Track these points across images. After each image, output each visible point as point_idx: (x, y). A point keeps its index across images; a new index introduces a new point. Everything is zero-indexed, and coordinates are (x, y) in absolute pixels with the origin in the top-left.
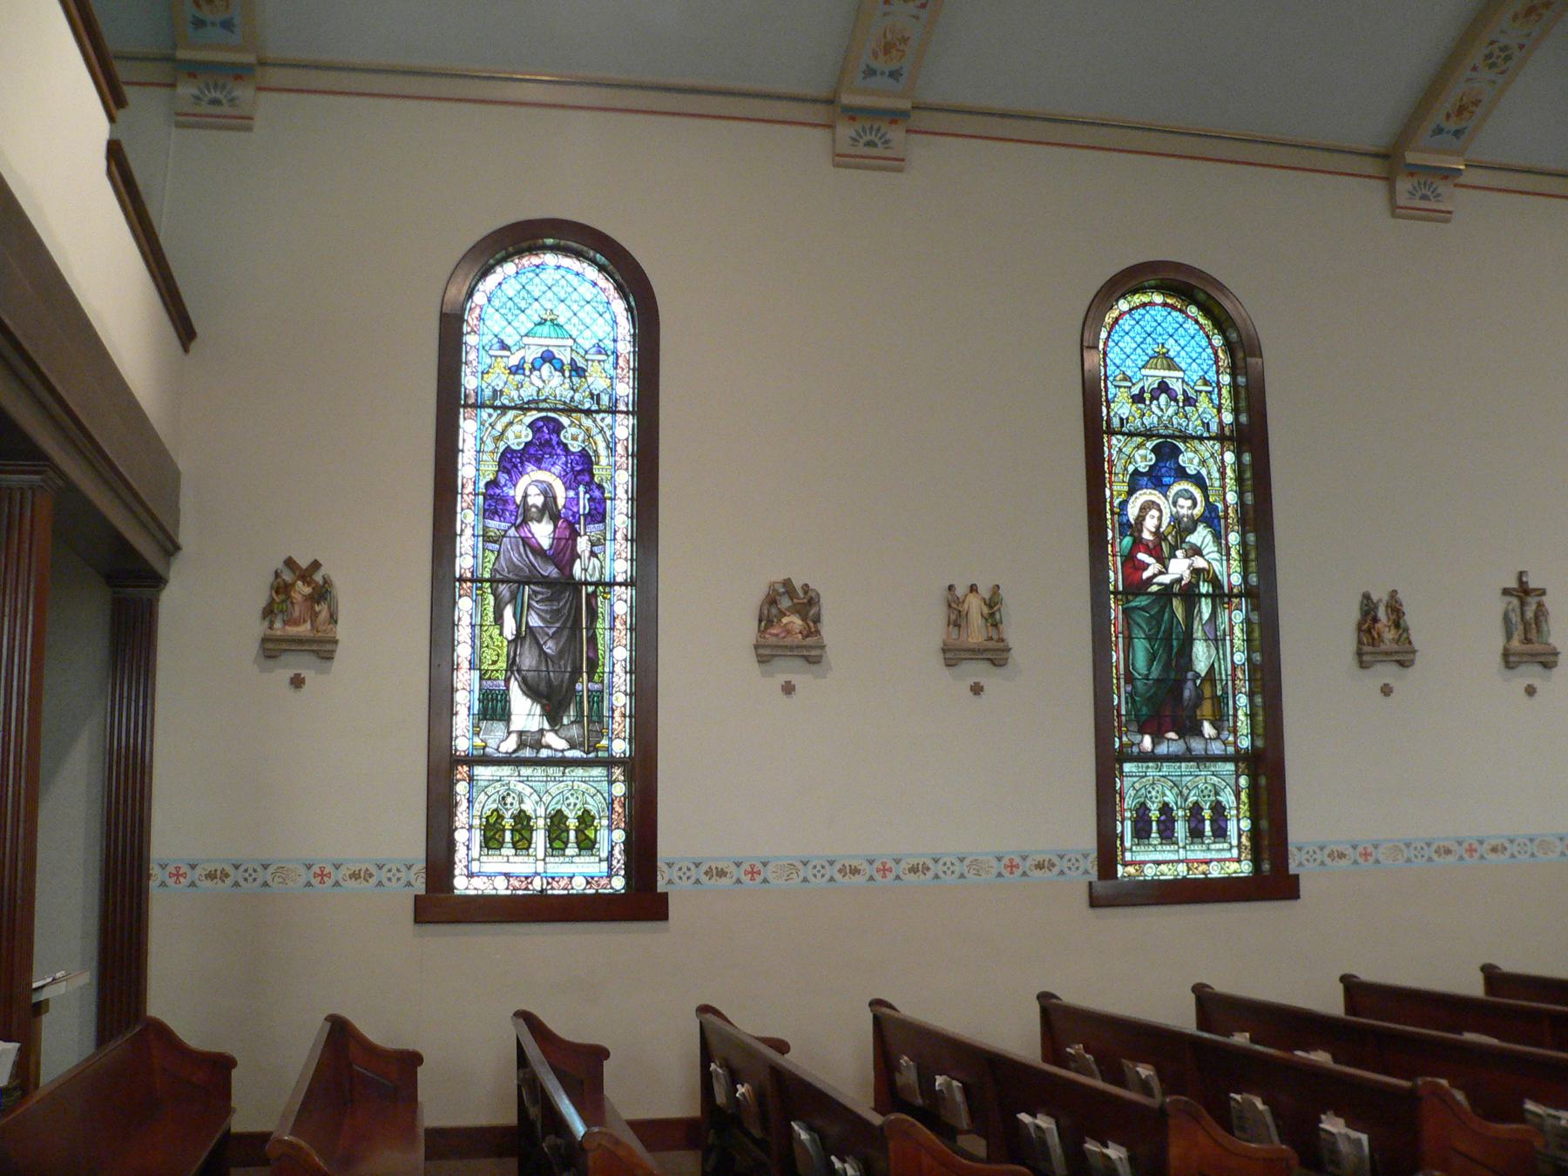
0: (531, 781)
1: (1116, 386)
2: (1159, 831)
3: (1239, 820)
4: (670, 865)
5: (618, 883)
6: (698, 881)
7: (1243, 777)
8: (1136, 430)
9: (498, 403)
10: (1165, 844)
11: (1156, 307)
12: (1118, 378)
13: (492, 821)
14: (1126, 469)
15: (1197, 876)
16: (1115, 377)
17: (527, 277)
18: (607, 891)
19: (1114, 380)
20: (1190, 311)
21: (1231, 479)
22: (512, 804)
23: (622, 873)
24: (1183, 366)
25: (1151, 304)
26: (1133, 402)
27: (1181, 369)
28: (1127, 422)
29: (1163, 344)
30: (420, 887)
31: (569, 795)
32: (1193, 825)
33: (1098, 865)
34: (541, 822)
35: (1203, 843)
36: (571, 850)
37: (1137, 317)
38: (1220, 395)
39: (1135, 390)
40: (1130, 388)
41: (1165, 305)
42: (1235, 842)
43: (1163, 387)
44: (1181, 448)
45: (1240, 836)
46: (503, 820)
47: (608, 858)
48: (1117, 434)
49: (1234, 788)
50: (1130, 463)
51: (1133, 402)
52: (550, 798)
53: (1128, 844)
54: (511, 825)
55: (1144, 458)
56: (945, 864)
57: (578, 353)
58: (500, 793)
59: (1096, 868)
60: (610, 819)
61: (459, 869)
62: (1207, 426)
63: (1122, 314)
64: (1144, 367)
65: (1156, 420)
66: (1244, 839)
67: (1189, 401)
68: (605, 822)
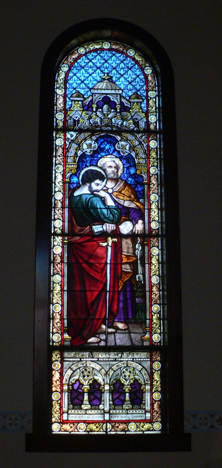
0: (101, 361)
1: (72, 101)
2: (90, 401)
3: (152, 394)
4: (194, 416)
5: (157, 426)
6: (212, 427)
7: (156, 363)
9: (77, 127)
11: (105, 52)
12: (74, 95)
13: (76, 387)
14: (76, 154)
15: (119, 433)
16: (72, 94)
17: (92, 55)
18: (101, 433)
19: (71, 97)
20: (130, 53)
23: (159, 420)
25: (102, 49)
28: (78, 123)
29: (108, 74)
30: (30, 429)
31: (124, 370)
34: (107, 387)
36: (86, 406)
38: (148, 104)
39: (87, 102)
41: (110, 50)
42: (148, 408)
45: (152, 405)
46: (82, 387)
47: (150, 411)
48: (71, 130)
49: (149, 370)
50: (79, 149)
52: (113, 372)
55: (90, 146)
60: (152, 386)
61: (55, 417)
62: (136, 123)
63: (80, 56)
66: (156, 406)
67: (127, 109)
68: (148, 387)
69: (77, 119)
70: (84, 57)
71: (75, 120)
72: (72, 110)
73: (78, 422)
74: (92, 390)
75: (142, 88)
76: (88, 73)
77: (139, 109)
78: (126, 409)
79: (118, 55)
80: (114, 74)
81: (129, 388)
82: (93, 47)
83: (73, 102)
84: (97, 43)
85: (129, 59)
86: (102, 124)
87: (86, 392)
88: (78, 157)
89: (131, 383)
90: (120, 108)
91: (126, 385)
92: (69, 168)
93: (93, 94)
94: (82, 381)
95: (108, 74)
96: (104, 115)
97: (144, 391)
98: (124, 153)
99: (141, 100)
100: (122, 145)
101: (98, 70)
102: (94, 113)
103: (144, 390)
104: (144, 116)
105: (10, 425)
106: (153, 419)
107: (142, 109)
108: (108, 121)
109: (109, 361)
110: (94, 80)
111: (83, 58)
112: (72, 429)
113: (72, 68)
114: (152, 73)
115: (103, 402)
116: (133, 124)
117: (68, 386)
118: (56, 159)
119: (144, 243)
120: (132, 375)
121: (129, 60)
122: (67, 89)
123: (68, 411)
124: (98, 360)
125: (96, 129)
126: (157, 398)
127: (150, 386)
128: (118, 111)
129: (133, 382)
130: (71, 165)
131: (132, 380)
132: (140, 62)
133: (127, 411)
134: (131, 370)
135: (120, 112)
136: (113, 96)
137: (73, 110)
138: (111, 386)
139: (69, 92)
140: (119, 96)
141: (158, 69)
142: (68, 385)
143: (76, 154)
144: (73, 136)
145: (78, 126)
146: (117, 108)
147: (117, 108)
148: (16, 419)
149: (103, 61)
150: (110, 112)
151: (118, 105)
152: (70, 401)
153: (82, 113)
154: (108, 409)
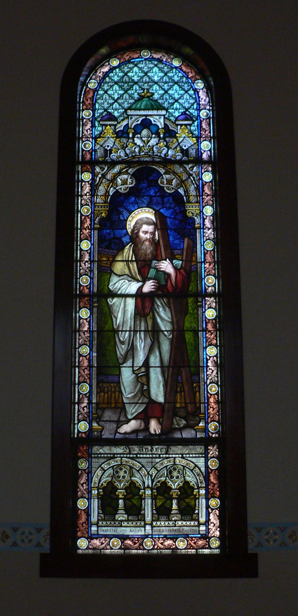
0: (140, 458)
1: (102, 125)
8: (133, 157)
10: (132, 521)
14: (107, 192)
19: (101, 120)
21: (208, 195)
22: (124, 477)
24: (166, 105)
26: (117, 137)
27: (163, 108)
28: (111, 153)
32: (159, 503)
33: (50, 539)
34: (148, 492)
35: (169, 520)
36: (121, 516)
37: (126, 70)
39: (120, 127)
40: (115, 125)
43: (146, 124)
44: (161, 171)
45: (208, 515)
51: (117, 137)
53: (94, 518)
54: (177, 495)
56: (23, 533)
57: (170, 120)
58: (168, 468)
59: (48, 541)
60: (207, 488)
63: (112, 69)
64: (130, 108)
65: (137, 150)
68: (203, 492)
69: (108, 149)
70: (117, 70)
71: (106, 149)
72: (102, 137)
73: (111, 537)
74: (128, 496)
75: (172, 107)
76: (183, 89)
77: (189, 134)
78: (120, 520)
79: (160, 65)
80: (156, 91)
81: (124, 493)
82: (128, 57)
83: (104, 127)
84: (134, 51)
85: (174, 70)
86: (140, 153)
87: (174, 498)
88: (110, 195)
89: (103, 486)
90: (163, 132)
91: (173, 489)
92: (99, 210)
93: (128, 115)
94: (116, 484)
95: (148, 89)
96: (144, 141)
97: (143, 497)
98: (170, 189)
99: (190, 122)
100: (166, 179)
101: (176, 85)
102: (130, 141)
103: (144, 495)
104: (195, 141)
105: (268, 541)
106: (209, 533)
107: (192, 133)
108: (149, 149)
109: (152, 458)
110: (130, 98)
111: (116, 71)
112: (103, 546)
113: (103, 84)
114: (205, 87)
115: (144, 511)
116: (181, 153)
117: (98, 490)
118: (82, 198)
119: (97, 304)
120: (181, 477)
121: (175, 71)
122: (97, 110)
123: (98, 523)
124: (137, 457)
125: (133, 160)
126: (83, 506)
127: (205, 490)
128: (162, 136)
129: (106, 485)
130: (101, 206)
131: (128, 482)
132: (190, 73)
133: (175, 522)
134: (127, 471)
135: (164, 138)
136: (154, 118)
137: (103, 137)
138: (100, 490)
139: (99, 114)
140: (162, 117)
141: (212, 83)
142: (98, 489)
143: (107, 192)
144: (104, 169)
145: (110, 157)
146: (160, 132)
147: (160, 132)
148: (275, 533)
149: (141, 74)
150: (151, 138)
151: (161, 129)
152: (154, 510)
153: (115, 140)
154: (96, 520)
